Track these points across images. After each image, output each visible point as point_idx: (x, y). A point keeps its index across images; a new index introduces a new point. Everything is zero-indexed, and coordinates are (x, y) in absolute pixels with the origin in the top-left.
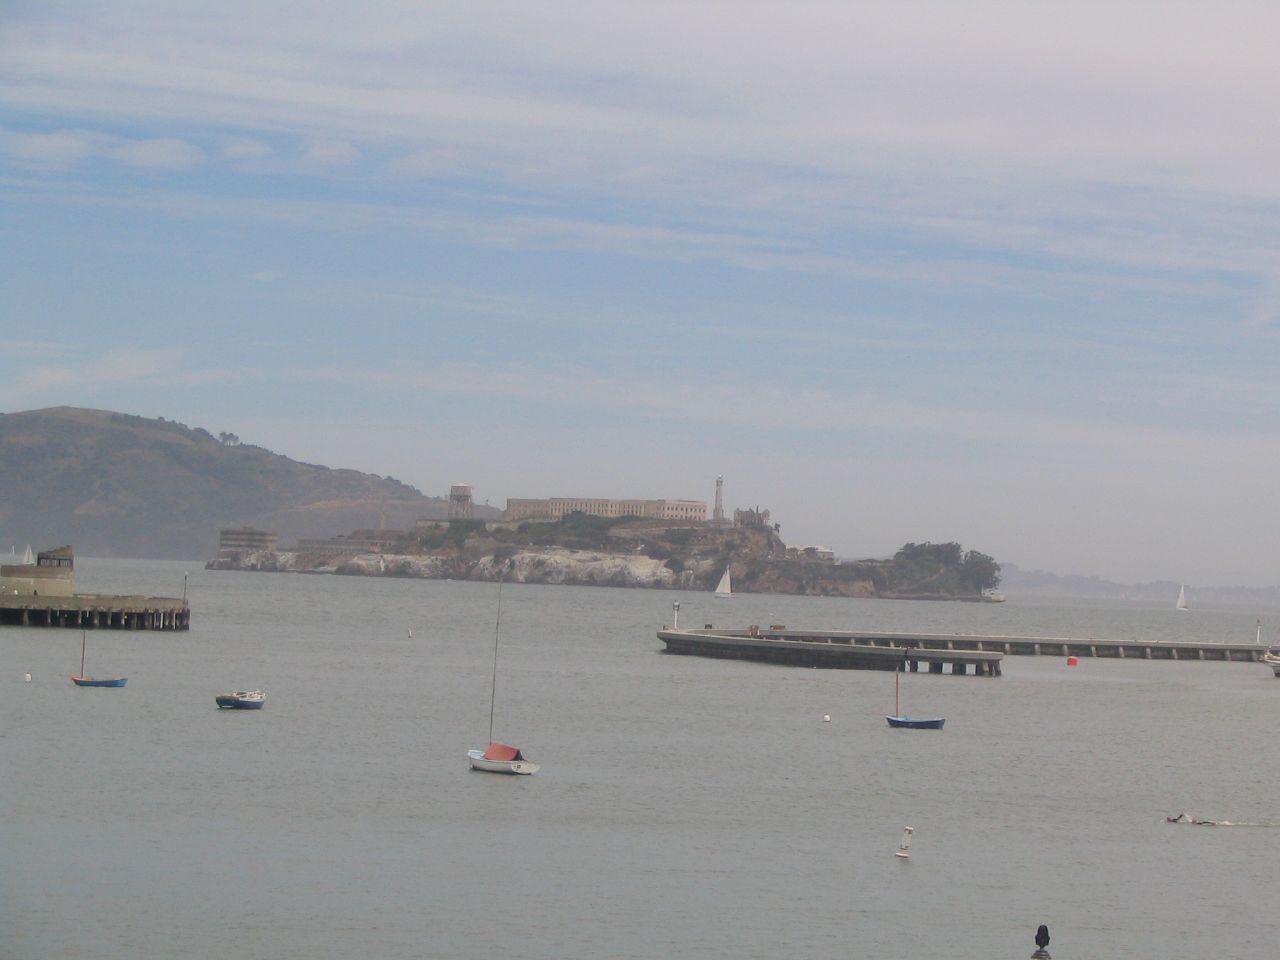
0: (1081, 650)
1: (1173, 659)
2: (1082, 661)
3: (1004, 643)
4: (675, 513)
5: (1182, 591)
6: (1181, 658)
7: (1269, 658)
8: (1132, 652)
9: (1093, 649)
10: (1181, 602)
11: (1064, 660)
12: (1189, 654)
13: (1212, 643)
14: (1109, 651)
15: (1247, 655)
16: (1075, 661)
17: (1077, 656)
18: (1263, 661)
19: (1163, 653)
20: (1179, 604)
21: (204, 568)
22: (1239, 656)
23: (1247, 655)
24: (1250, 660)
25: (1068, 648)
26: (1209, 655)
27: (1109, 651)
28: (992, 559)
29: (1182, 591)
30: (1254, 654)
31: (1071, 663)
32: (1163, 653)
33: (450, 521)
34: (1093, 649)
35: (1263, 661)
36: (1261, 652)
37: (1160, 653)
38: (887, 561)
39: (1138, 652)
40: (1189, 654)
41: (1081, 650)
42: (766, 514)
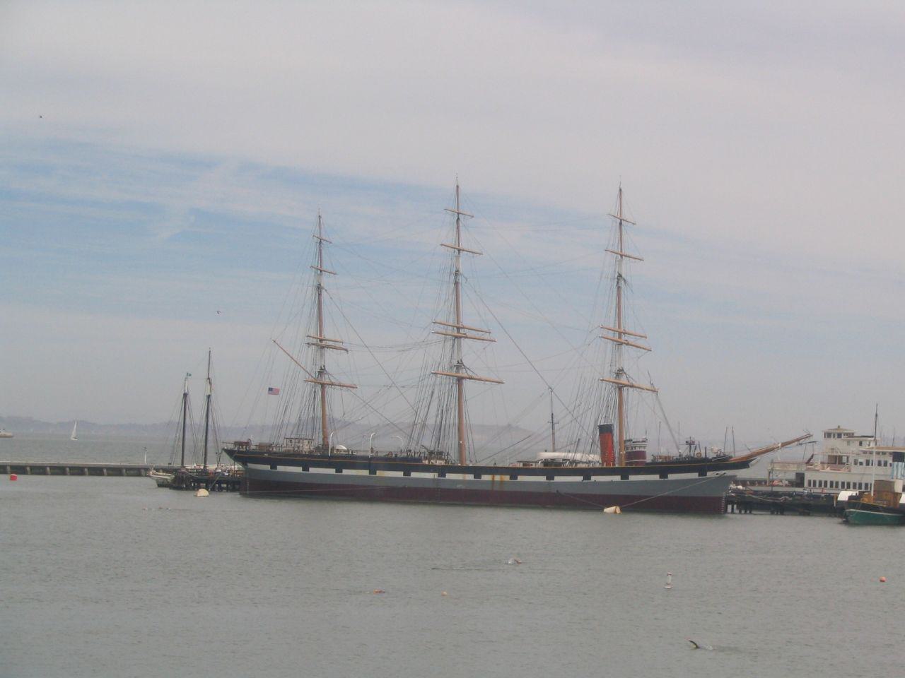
0: (20, 470)
1: (142, 476)
2: (20, 477)
3: (26, 466)
4: (817, 491)
5: (75, 426)
6: (91, 474)
7: (153, 474)
8: (56, 471)
9: (28, 469)
10: (74, 433)
11: (7, 477)
12: (97, 471)
13: (16, 461)
14: (39, 470)
15: (138, 472)
16: (544, 466)
17: (17, 473)
18: (149, 476)
19: (78, 471)
20: (72, 436)
21: (251, 438)
22: (132, 472)
23: (138, 472)
24: (139, 475)
25: (70, 470)
26: (110, 472)
27: (39, 470)
28: (736, 476)
29: (75, 426)
30: (143, 471)
31: (13, 479)
32: (78, 471)
33: (789, 482)
34: (28, 469)
35: (149, 476)
36: (147, 469)
37: (76, 471)
38: (894, 488)
39: (59, 470)
40: (97, 471)
41: (20, 470)
42: (736, 476)
